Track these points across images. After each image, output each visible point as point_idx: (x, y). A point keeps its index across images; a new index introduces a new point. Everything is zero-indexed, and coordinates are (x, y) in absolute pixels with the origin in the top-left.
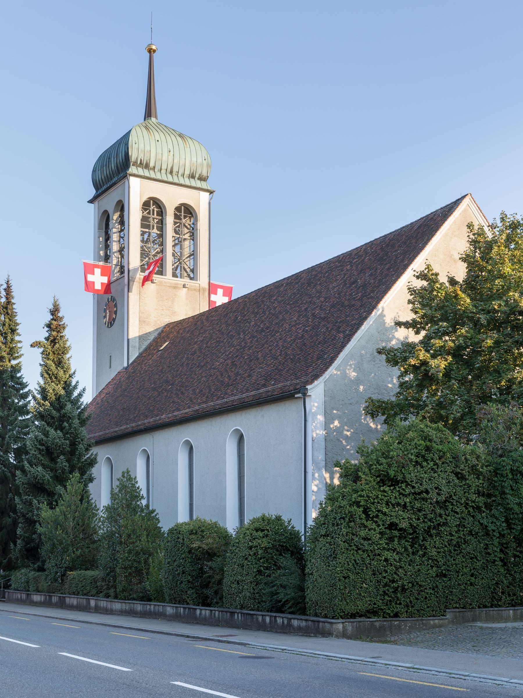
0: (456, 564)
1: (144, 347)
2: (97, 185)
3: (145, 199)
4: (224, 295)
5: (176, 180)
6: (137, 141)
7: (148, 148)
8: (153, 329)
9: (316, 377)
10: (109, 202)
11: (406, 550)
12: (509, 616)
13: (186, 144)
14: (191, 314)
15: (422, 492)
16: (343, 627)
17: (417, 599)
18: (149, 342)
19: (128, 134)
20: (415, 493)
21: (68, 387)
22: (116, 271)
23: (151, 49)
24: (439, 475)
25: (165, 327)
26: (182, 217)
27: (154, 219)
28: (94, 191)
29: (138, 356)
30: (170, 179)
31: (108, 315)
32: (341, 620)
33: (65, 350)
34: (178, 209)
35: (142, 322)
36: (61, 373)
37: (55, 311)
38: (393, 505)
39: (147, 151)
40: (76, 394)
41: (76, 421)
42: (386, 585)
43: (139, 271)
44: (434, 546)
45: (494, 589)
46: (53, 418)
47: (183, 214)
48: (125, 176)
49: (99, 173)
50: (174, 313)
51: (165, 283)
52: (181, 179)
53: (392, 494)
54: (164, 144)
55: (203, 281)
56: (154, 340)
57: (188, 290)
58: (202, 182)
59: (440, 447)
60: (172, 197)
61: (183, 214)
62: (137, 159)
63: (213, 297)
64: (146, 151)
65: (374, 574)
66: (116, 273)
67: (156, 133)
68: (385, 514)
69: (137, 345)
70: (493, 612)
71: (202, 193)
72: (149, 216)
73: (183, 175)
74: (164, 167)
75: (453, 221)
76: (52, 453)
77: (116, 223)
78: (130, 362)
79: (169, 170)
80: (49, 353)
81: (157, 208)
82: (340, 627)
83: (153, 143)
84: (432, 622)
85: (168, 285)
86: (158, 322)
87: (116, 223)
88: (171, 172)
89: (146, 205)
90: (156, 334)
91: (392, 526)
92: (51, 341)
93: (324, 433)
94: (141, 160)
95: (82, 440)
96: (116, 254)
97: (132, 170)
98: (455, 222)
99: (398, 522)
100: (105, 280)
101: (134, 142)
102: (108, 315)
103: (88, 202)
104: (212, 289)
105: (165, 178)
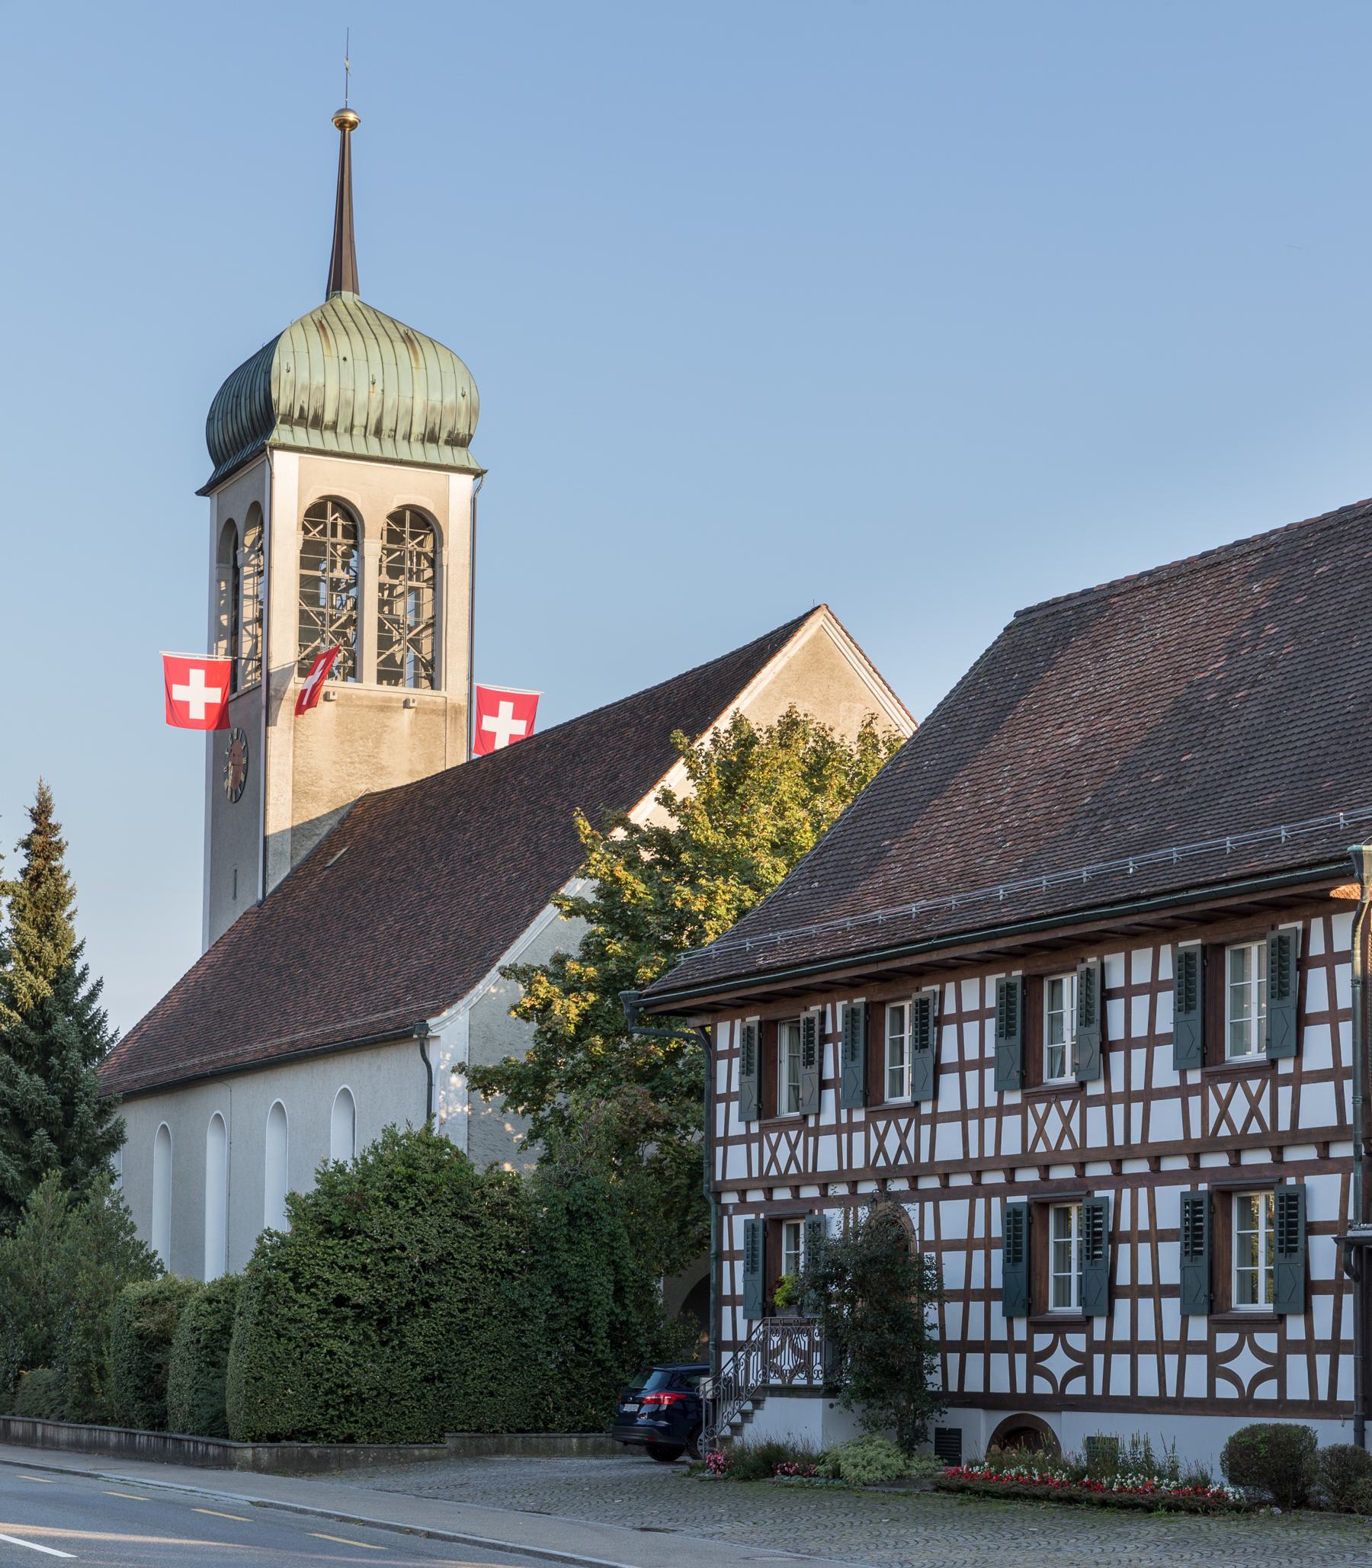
0: (461, 1362)
1: (304, 853)
2: (217, 454)
3: (311, 499)
4: (516, 716)
5: (389, 453)
6: (292, 366)
7: (318, 380)
8: (326, 811)
9: (456, 998)
10: (239, 494)
11: (368, 1337)
12: (571, 1448)
13: (417, 360)
14: (424, 772)
15: (392, 1248)
16: (254, 1455)
17: (388, 1415)
18: (316, 840)
19: (268, 351)
20: (380, 1249)
21: (65, 979)
22: (249, 668)
23: (345, 121)
24: (426, 1222)
25: (355, 805)
26: (406, 536)
27: (334, 546)
28: (210, 468)
29: (288, 876)
30: (375, 451)
31: (231, 772)
32: (250, 1444)
33: (60, 899)
34: (396, 517)
35: (299, 793)
36: (49, 947)
37: (41, 813)
38: (343, 1269)
39: (317, 388)
40: (83, 991)
41: (75, 1054)
42: (330, 1391)
43: (296, 675)
44: (418, 1333)
45: (537, 1403)
46: (28, 1046)
47: (407, 529)
48: (262, 453)
49: (218, 425)
50: (380, 769)
51: (359, 698)
52: (403, 445)
53: (341, 1250)
54: (361, 364)
55: (455, 687)
56: (328, 836)
57: (417, 712)
58: (457, 450)
59: (428, 1177)
60: (377, 491)
61: (407, 529)
62: (292, 407)
63: (488, 723)
64: (313, 387)
65: (308, 1375)
66: (251, 673)
67: (343, 340)
68: (327, 1282)
69: (288, 848)
70: (534, 1438)
71: (455, 478)
72: (323, 539)
73: (408, 437)
74: (360, 421)
75: (783, 664)
76: (24, 1123)
77: (250, 553)
78: (270, 889)
79: (372, 426)
80: (25, 906)
81: (343, 518)
82: (249, 1453)
83: (332, 365)
84: (417, 1452)
85: (365, 703)
86: (341, 792)
87: (250, 553)
88: (378, 432)
89: (315, 513)
90: (334, 822)
91: (341, 1301)
92: (31, 879)
93: (466, 1109)
94: (302, 409)
95: (87, 1095)
96: (249, 628)
97: (281, 433)
98: (788, 666)
99: (350, 1294)
100: (215, 695)
101: (284, 368)
102: (231, 772)
103: (198, 493)
104: (485, 702)
105: (361, 450)
